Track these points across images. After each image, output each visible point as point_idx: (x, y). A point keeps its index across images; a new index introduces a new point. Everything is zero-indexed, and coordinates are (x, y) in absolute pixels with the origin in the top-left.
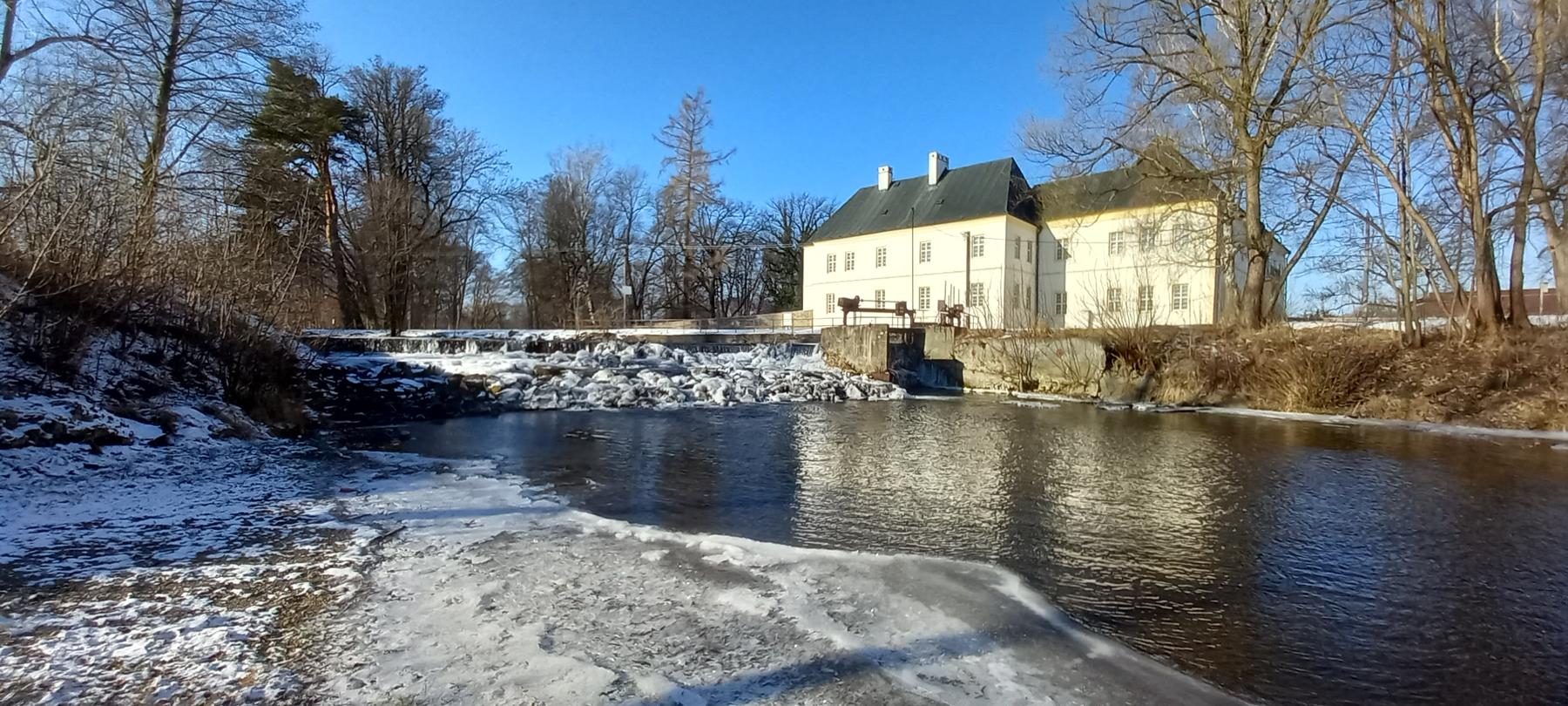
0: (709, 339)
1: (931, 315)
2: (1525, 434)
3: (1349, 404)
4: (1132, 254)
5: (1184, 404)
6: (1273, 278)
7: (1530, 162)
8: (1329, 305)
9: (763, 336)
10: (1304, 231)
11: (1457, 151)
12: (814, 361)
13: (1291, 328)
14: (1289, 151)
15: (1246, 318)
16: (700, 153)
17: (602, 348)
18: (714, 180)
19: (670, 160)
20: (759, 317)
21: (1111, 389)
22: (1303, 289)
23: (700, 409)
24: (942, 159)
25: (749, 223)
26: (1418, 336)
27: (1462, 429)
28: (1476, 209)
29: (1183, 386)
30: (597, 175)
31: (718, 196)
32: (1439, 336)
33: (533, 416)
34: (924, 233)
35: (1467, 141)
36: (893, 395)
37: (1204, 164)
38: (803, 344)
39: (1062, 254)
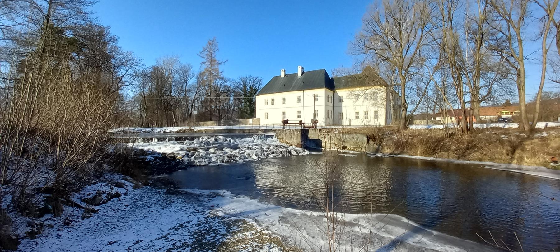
5: (390, 154)
12: (275, 141)
17: (203, 139)
19: (204, 63)
21: (368, 148)
24: (302, 68)
30: (175, 67)
31: (221, 76)
33: (204, 168)
34: (300, 93)
39: (341, 101)
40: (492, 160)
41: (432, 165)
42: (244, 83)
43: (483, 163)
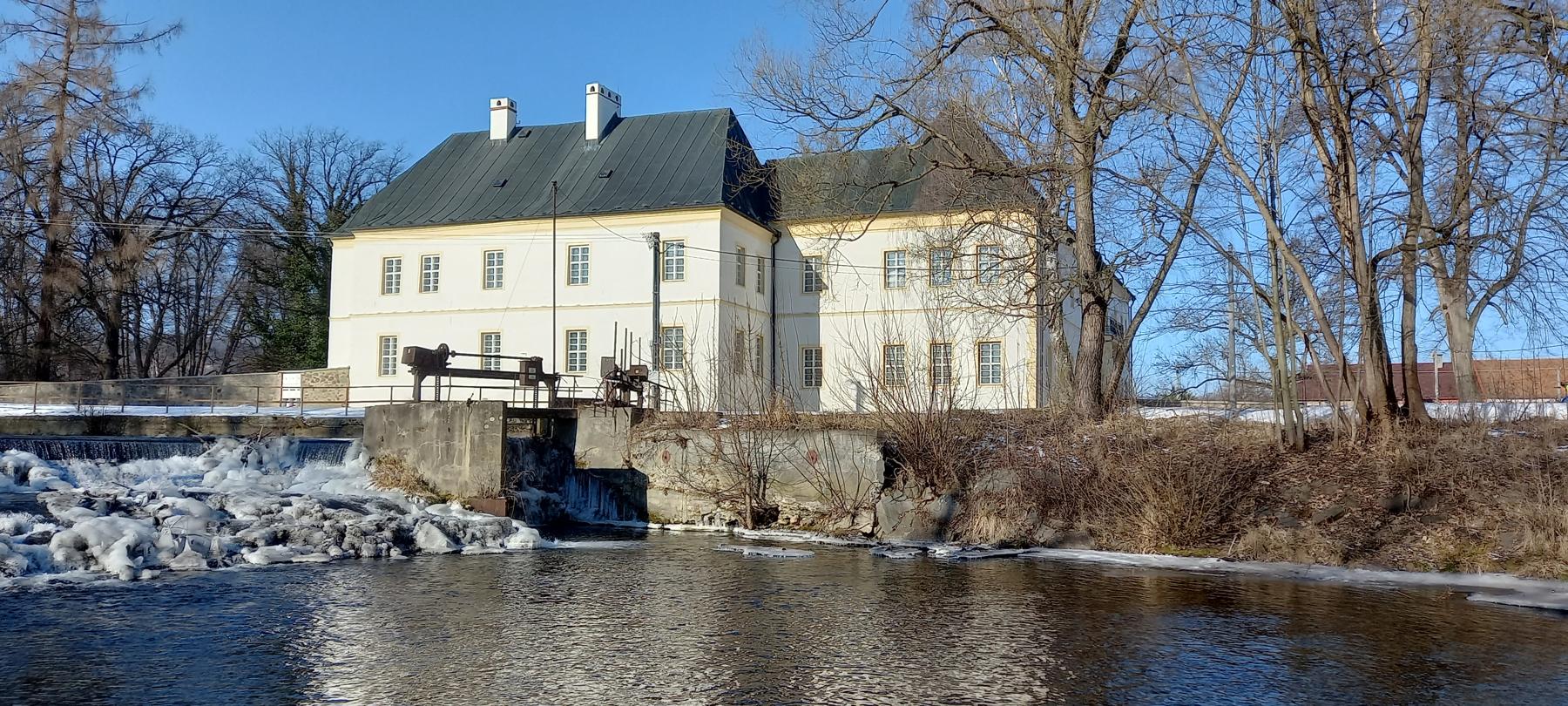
0: (98, 425)
1: (589, 384)
2: (1434, 578)
3: (1224, 539)
4: (919, 290)
5: (1003, 545)
6: (1116, 338)
7: (1416, 186)
8: (1187, 380)
9: (234, 422)
10: (1153, 268)
11: (1334, 170)
12: (350, 476)
13: (1140, 420)
14: (1132, 146)
15: (1084, 401)
16: (94, 23)
18: (126, 80)
20: (227, 379)
21: (897, 521)
22: (1153, 354)
23: (68, 591)
24: (606, 95)
25: (209, 181)
26: (1300, 435)
27: (1362, 575)
28: (1358, 250)
29: (999, 514)
31: (134, 117)
32: (1324, 435)
34: (575, 231)
35: (1344, 158)
36: (514, 542)
37: (1019, 154)
38: (329, 438)
39: (813, 283)
40: (1505, 563)
41: (1211, 598)
42: (291, 171)
43: (1466, 580)
